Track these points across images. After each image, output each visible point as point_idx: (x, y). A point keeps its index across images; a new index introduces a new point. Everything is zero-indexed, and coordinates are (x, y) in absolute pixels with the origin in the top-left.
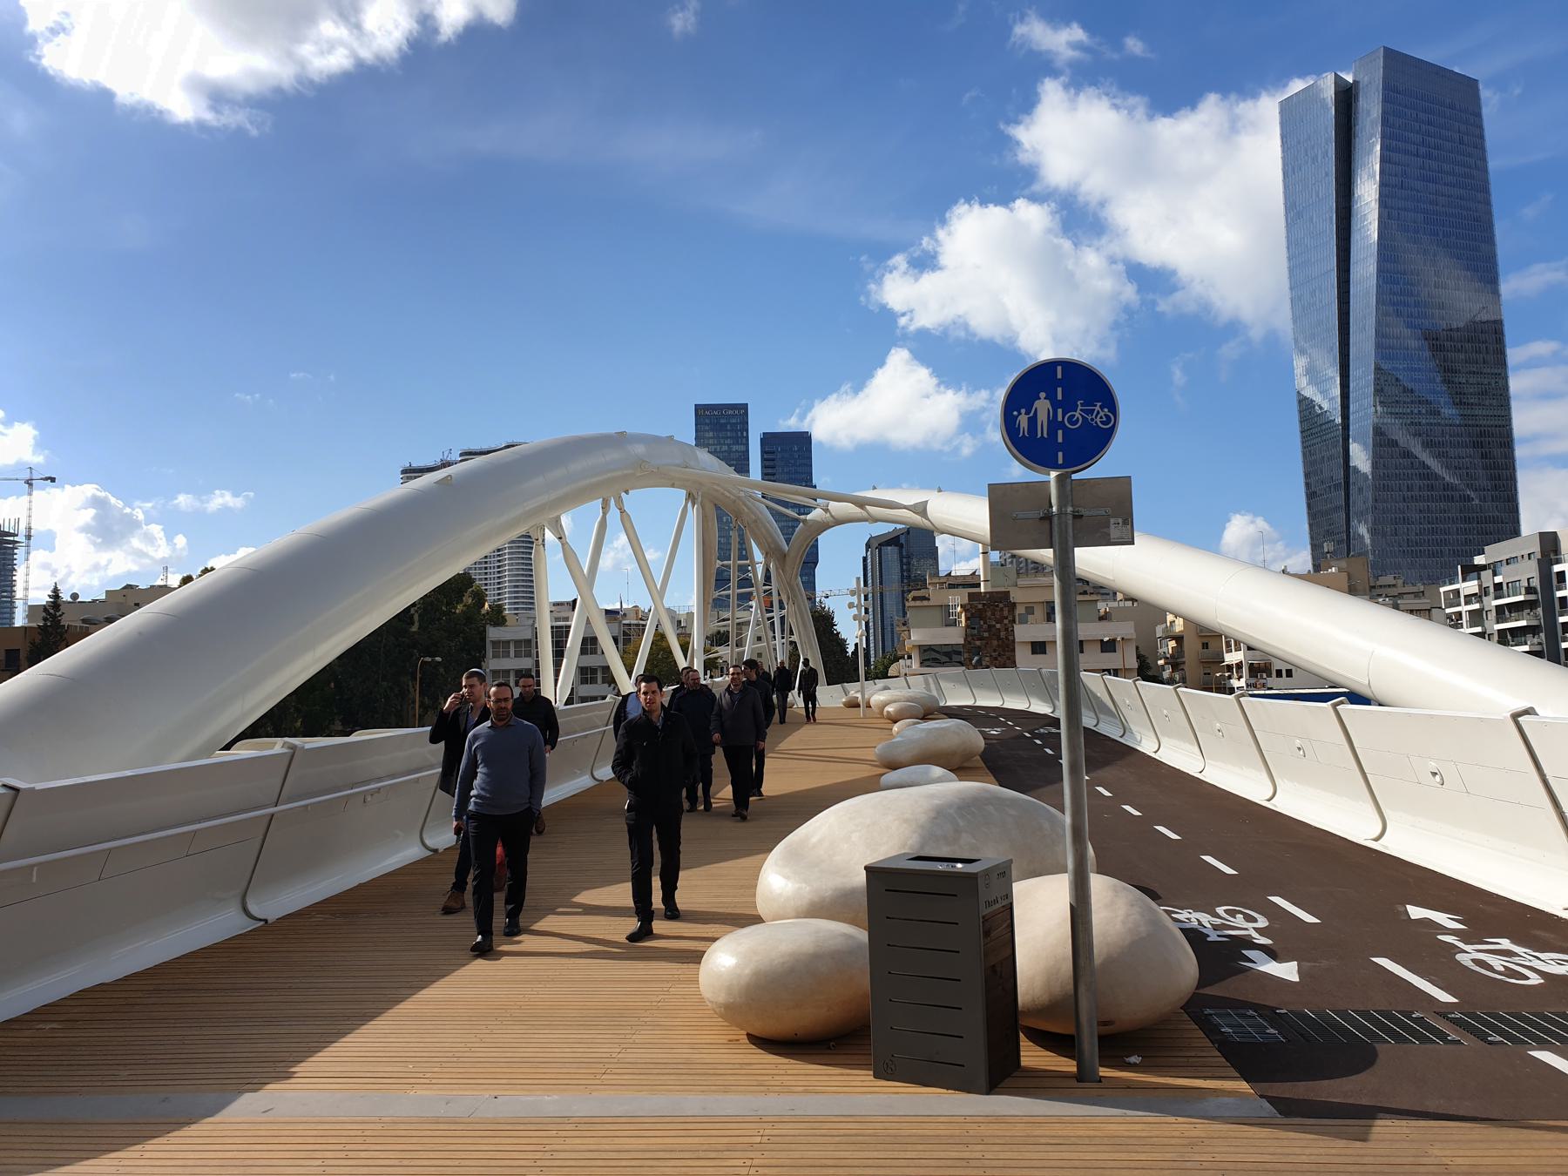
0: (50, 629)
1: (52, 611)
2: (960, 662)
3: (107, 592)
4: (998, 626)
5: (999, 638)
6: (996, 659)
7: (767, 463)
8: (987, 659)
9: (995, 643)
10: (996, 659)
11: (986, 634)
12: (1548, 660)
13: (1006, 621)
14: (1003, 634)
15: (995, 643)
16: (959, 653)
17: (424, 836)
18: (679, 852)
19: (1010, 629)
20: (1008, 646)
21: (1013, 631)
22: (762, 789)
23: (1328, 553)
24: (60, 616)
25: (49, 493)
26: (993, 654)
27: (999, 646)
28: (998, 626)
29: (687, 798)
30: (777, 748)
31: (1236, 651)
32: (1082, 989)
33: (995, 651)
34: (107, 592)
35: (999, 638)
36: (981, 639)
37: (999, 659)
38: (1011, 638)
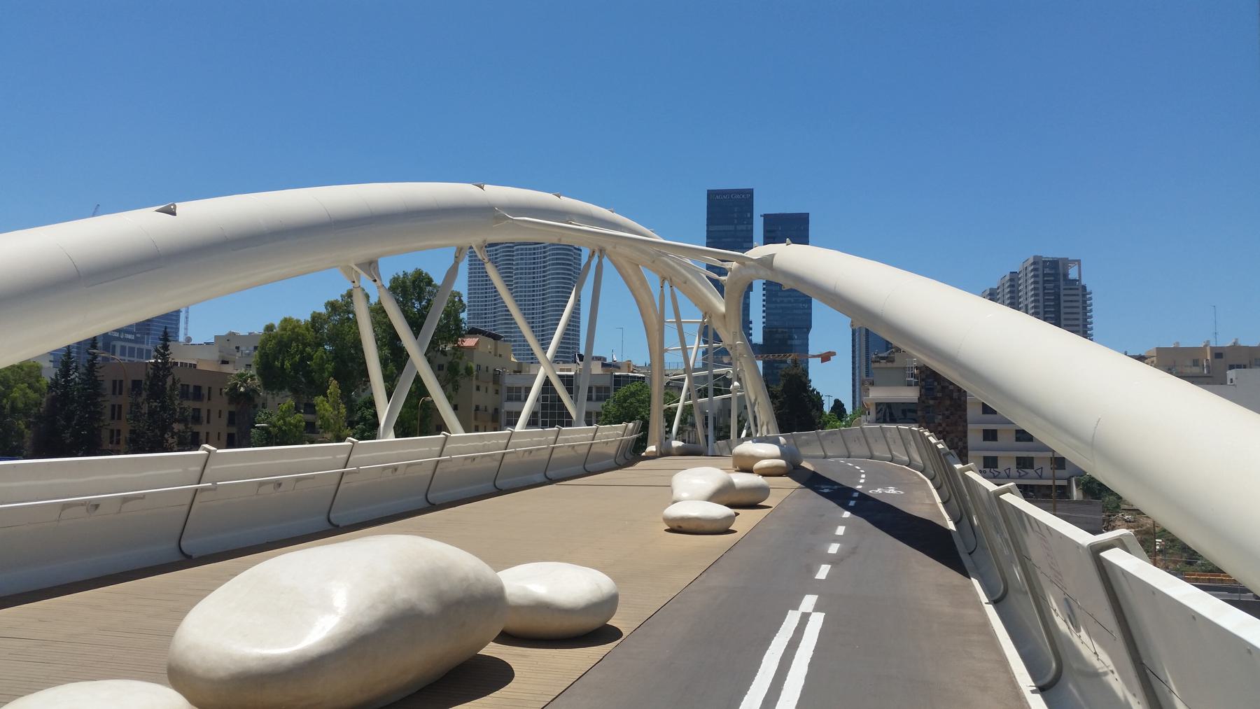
0: (161, 366)
1: (162, 351)
2: (914, 420)
3: (216, 337)
5: (951, 399)
6: (948, 417)
7: (577, 342)
8: (940, 417)
9: (948, 402)
10: (948, 417)
11: (939, 395)
15: (948, 402)
16: (915, 411)
18: (746, 694)
23: (339, 412)
24: (168, 354)
25: (397, 274)
26: (946, 413)
30: (644, 454)
31: (188, 386)
33: (947, 410)
34: (216, 337)
35: (951, 399)
36: (935, 398)
37: (951, 417)
38: (963, 398)
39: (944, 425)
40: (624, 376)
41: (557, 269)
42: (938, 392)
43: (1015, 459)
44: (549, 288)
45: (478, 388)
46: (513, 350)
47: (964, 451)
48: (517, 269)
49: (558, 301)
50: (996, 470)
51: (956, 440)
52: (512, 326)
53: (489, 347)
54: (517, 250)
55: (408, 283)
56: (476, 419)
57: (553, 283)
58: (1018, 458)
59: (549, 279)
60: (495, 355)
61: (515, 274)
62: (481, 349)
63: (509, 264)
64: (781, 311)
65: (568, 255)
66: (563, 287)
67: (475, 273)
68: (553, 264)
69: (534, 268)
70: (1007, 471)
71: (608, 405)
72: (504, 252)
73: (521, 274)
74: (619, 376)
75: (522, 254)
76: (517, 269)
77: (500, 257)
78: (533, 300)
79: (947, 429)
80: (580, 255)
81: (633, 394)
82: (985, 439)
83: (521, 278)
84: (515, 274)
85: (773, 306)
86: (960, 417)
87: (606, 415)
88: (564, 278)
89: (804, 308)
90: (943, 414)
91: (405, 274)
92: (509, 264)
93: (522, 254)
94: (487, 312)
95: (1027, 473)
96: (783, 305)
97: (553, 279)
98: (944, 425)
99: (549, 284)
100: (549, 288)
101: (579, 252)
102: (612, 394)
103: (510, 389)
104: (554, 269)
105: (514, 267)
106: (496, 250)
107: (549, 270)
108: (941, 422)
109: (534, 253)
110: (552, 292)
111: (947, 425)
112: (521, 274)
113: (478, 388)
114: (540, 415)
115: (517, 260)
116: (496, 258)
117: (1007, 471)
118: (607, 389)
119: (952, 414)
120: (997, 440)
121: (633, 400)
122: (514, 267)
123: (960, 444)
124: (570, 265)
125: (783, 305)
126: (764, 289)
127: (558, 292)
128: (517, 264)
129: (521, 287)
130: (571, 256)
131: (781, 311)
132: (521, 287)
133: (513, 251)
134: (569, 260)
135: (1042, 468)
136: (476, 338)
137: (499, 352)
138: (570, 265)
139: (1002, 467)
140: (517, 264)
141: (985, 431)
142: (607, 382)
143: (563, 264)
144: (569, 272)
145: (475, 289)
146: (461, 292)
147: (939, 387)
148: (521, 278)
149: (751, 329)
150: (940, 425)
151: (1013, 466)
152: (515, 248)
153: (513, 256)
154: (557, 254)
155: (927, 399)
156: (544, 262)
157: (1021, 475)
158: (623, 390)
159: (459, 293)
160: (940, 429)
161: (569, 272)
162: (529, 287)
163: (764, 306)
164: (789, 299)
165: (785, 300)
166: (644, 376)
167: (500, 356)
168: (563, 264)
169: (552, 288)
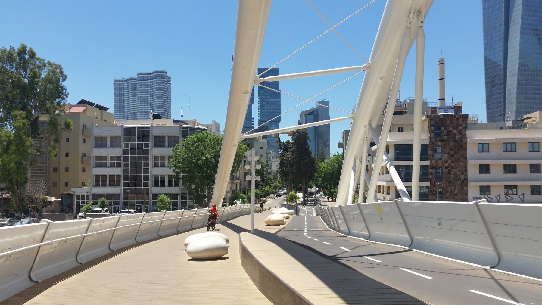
4: (455, 131)
6: (452, 155)
9: (452, 143)
10: (452, 155)
11: (445, 137)
12: (280, 113)
13: (460, 128)
14: (458, 137)
15: (452, 143)
17: (497, 260)
19: (463, 134)
20: (461, 146)
21: (465, 135)
22: (219, 224)
25: (3, 47)
27: (455, 146)
28: (455, 131)
29: (398, 236)
32: (340, 266)
33: (452, 149)
35: (455, 140)
36: (442, 140)
37: (455, 155)
38: (464, 140)
39: (449, 162)
40: (190, 128)
41: (159, 92)
42: (445, 135)
43: (504, 186)
44: (155, 102)
45: (85, 141)
46: (115, 118)
47: (465, 182)
48: (139, 92)
49: (160, 108)
50: (489, 196)
51: (459, 173)
52: (137, 118)
53: (96, 114)
54: (139, 83)
55: (15, 55)
56: (82, 163)
57: (157, 99)
58: (481, 187)
59: (155, 97)
60: (102, 120)
61: (138, 95)
62: (88, 114)
63: (135, 90)
64: (266, 114)
65: (164, 86)
66: (162, 102)
67: (117, 94)
68: (157, 90)
69: (147, 92)
70: (498, 197)
71: (178, 149)
72: (132, 84)
73: (141, 94)
74: (187, 128)
75: (141, 85)
76: (139, 92)
77: (130, 86)
78: (147, 107)
79: (452, 164)
80: (170, 86)
81: (199, 140)
82: (481, 172)
83: (141, 97)
84: (138, 95)
85: (263, 111)
86: (462, 155)
87: (176, 157)
88: (162, 97)
89: (277, 112)
90: (449, 153)
91: (12, 49)
92: (135, 90)
93: (141, 85)
94: (124, 113)
95: (512, 198)
96: (267, 111)
97: (157, 97)
98: (449, 162)
99: (155, 100)
100: (155, 102)
101: (170, 85)
102: (181, 141)
103: (97, 139)
104: (157, 93)
105: (137, 94)
106: (128, 83)
107: (155, 93)
108: (447, 159)
109: (147, 85)
110: (157, 104)
111: (452, 162)
112: (141, 94)
113: (85, 141)
114: (122, 159)
115: (139, 88)
116: (128, 87)
117: (498, 197)
118: (177, 138)
119: (455, 153)
120: (489, 173)
121: (198, 144)
122: (137, 91)
123: (462, 176)
124: (165, 91)
125: (267, 111)
126: (258, 104)
127: (160, 104)
128: (139, 90)
129: (141, 101)
130: (166, 86)
131: (266, 114)
132: (141, 101)
133: (136, 84)
134: (165, 88)
135: (523, 194)
136: (84, 107)
137: (104, 119)
138: (165, 91)
139: (493, 193)
140: (139, 90)
141: (505, 166)
142: (177, 132)
143: (162, 90)
144: (165, 94)
145: (117, 102)
146: (61, 65)
147: (445, 131)
148: (141, 97)
149: (253, 122)
150: (446, 161)
151: (502, 192)
152: (137, 82)
153: (136, 88)
154: (159, 85)
155: (436, 141)
156: (152, 89)
157: (508, 200)
158: (190, 138)
159: (60, 66)
160: (446, 164)
161: (165, 94)
162: (145, 101)
163: (258, 111)
164: (270, 108)
165: (269, 108)
166: (206, 128)
167: (105, 121)
168: (162, 90)
169: (157, 102)
